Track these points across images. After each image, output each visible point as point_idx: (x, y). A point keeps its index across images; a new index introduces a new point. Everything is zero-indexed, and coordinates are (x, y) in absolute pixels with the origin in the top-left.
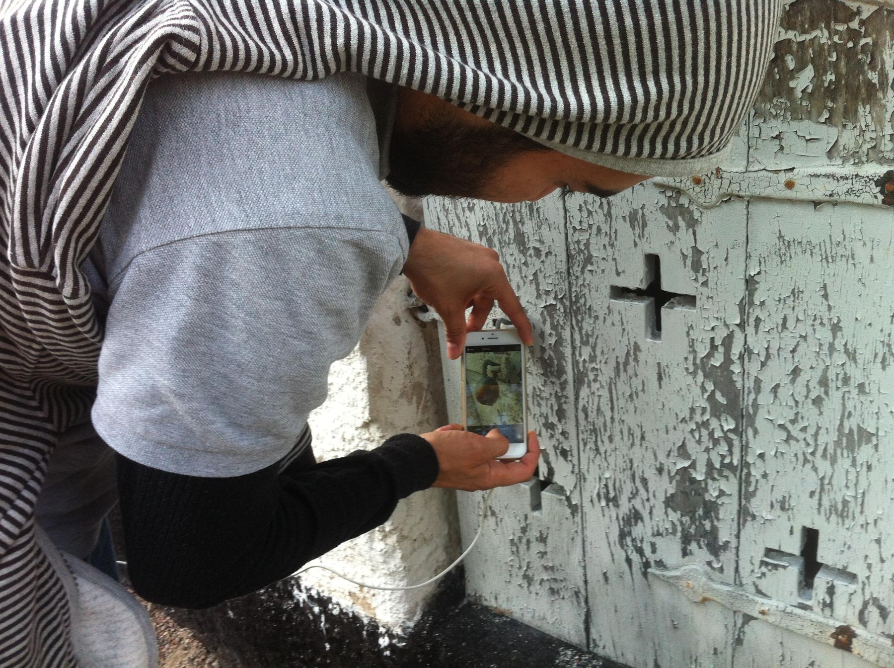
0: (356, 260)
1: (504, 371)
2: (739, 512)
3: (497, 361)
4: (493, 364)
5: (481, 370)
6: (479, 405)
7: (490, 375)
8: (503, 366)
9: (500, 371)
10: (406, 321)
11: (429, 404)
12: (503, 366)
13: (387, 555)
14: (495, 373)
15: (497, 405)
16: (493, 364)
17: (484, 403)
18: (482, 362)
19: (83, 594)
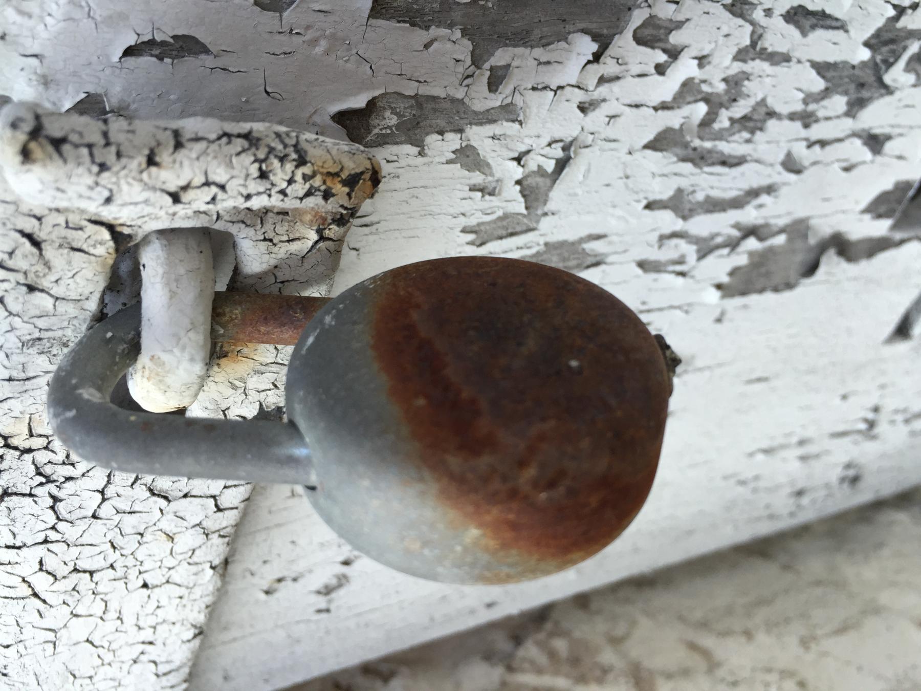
0: (505, 546)
1: (214, 182)
2: (819, 73)
3: (81, 281)
4: (117, 325)
5: (202, 499)
6: (649, 537)
7: (257, 380)
8: (139, 203)
9: (210, 242)
10: (444, 598)
11: (560, 645)
12: (139, 203)
13: (158, 257)
14: (238, 307)
15: (675, 306)
16: (117, 325)
17: (620, 489)
18: (87, 479)
19: (419, 144)
